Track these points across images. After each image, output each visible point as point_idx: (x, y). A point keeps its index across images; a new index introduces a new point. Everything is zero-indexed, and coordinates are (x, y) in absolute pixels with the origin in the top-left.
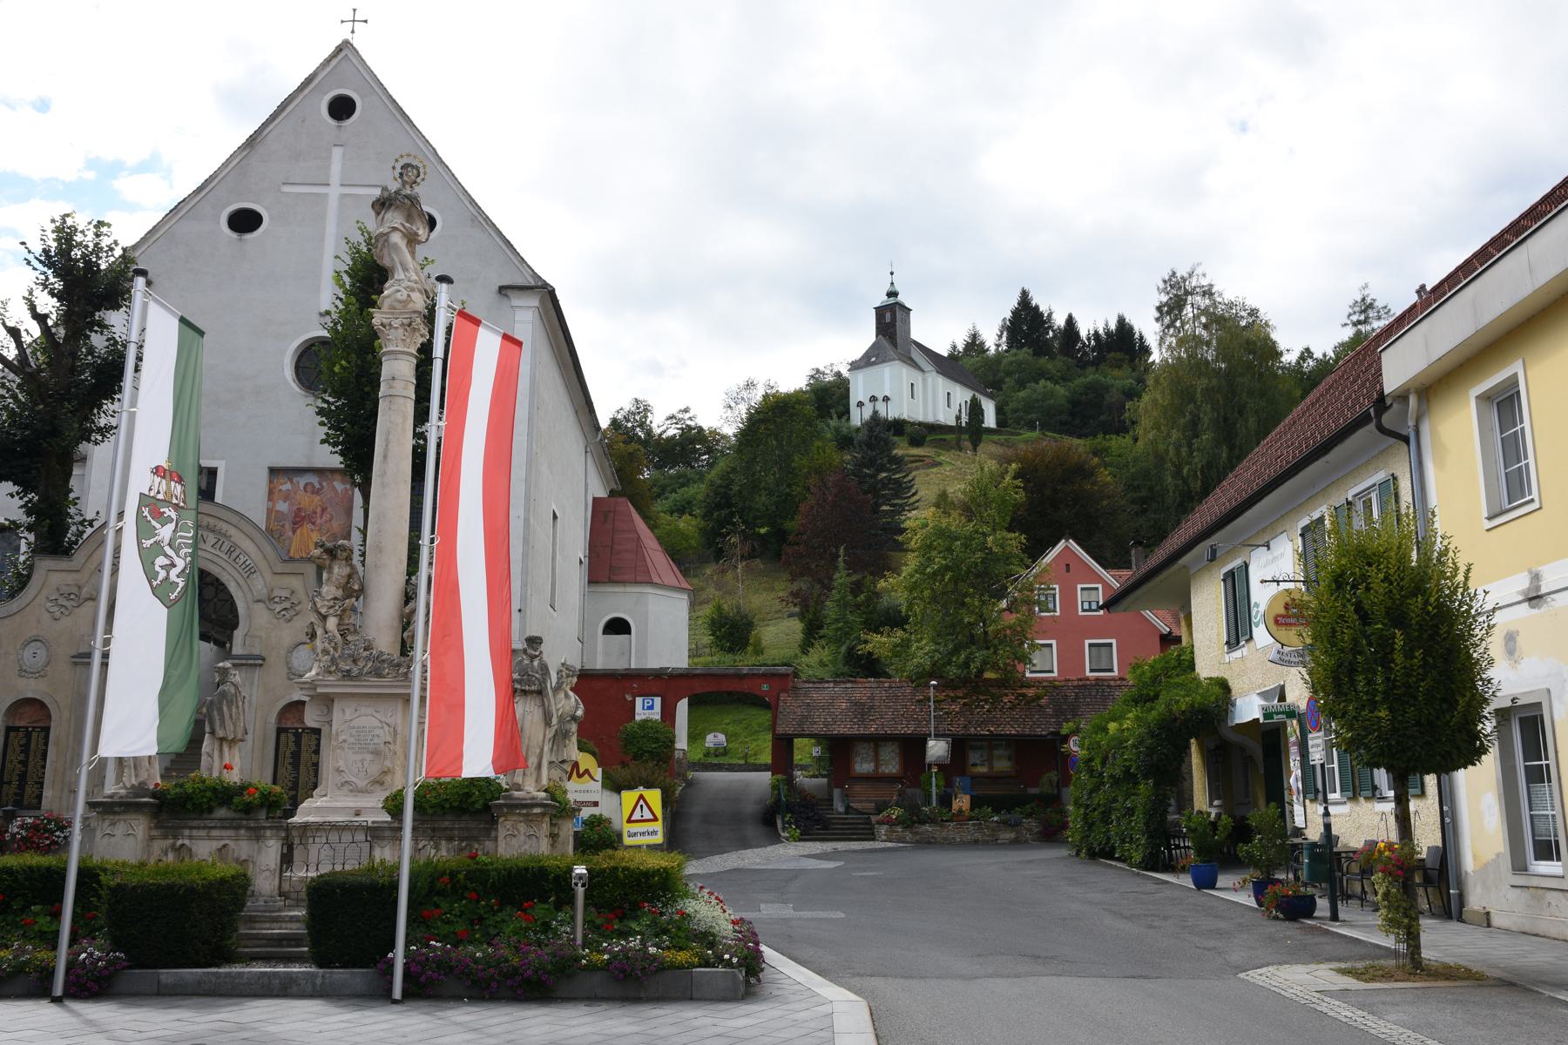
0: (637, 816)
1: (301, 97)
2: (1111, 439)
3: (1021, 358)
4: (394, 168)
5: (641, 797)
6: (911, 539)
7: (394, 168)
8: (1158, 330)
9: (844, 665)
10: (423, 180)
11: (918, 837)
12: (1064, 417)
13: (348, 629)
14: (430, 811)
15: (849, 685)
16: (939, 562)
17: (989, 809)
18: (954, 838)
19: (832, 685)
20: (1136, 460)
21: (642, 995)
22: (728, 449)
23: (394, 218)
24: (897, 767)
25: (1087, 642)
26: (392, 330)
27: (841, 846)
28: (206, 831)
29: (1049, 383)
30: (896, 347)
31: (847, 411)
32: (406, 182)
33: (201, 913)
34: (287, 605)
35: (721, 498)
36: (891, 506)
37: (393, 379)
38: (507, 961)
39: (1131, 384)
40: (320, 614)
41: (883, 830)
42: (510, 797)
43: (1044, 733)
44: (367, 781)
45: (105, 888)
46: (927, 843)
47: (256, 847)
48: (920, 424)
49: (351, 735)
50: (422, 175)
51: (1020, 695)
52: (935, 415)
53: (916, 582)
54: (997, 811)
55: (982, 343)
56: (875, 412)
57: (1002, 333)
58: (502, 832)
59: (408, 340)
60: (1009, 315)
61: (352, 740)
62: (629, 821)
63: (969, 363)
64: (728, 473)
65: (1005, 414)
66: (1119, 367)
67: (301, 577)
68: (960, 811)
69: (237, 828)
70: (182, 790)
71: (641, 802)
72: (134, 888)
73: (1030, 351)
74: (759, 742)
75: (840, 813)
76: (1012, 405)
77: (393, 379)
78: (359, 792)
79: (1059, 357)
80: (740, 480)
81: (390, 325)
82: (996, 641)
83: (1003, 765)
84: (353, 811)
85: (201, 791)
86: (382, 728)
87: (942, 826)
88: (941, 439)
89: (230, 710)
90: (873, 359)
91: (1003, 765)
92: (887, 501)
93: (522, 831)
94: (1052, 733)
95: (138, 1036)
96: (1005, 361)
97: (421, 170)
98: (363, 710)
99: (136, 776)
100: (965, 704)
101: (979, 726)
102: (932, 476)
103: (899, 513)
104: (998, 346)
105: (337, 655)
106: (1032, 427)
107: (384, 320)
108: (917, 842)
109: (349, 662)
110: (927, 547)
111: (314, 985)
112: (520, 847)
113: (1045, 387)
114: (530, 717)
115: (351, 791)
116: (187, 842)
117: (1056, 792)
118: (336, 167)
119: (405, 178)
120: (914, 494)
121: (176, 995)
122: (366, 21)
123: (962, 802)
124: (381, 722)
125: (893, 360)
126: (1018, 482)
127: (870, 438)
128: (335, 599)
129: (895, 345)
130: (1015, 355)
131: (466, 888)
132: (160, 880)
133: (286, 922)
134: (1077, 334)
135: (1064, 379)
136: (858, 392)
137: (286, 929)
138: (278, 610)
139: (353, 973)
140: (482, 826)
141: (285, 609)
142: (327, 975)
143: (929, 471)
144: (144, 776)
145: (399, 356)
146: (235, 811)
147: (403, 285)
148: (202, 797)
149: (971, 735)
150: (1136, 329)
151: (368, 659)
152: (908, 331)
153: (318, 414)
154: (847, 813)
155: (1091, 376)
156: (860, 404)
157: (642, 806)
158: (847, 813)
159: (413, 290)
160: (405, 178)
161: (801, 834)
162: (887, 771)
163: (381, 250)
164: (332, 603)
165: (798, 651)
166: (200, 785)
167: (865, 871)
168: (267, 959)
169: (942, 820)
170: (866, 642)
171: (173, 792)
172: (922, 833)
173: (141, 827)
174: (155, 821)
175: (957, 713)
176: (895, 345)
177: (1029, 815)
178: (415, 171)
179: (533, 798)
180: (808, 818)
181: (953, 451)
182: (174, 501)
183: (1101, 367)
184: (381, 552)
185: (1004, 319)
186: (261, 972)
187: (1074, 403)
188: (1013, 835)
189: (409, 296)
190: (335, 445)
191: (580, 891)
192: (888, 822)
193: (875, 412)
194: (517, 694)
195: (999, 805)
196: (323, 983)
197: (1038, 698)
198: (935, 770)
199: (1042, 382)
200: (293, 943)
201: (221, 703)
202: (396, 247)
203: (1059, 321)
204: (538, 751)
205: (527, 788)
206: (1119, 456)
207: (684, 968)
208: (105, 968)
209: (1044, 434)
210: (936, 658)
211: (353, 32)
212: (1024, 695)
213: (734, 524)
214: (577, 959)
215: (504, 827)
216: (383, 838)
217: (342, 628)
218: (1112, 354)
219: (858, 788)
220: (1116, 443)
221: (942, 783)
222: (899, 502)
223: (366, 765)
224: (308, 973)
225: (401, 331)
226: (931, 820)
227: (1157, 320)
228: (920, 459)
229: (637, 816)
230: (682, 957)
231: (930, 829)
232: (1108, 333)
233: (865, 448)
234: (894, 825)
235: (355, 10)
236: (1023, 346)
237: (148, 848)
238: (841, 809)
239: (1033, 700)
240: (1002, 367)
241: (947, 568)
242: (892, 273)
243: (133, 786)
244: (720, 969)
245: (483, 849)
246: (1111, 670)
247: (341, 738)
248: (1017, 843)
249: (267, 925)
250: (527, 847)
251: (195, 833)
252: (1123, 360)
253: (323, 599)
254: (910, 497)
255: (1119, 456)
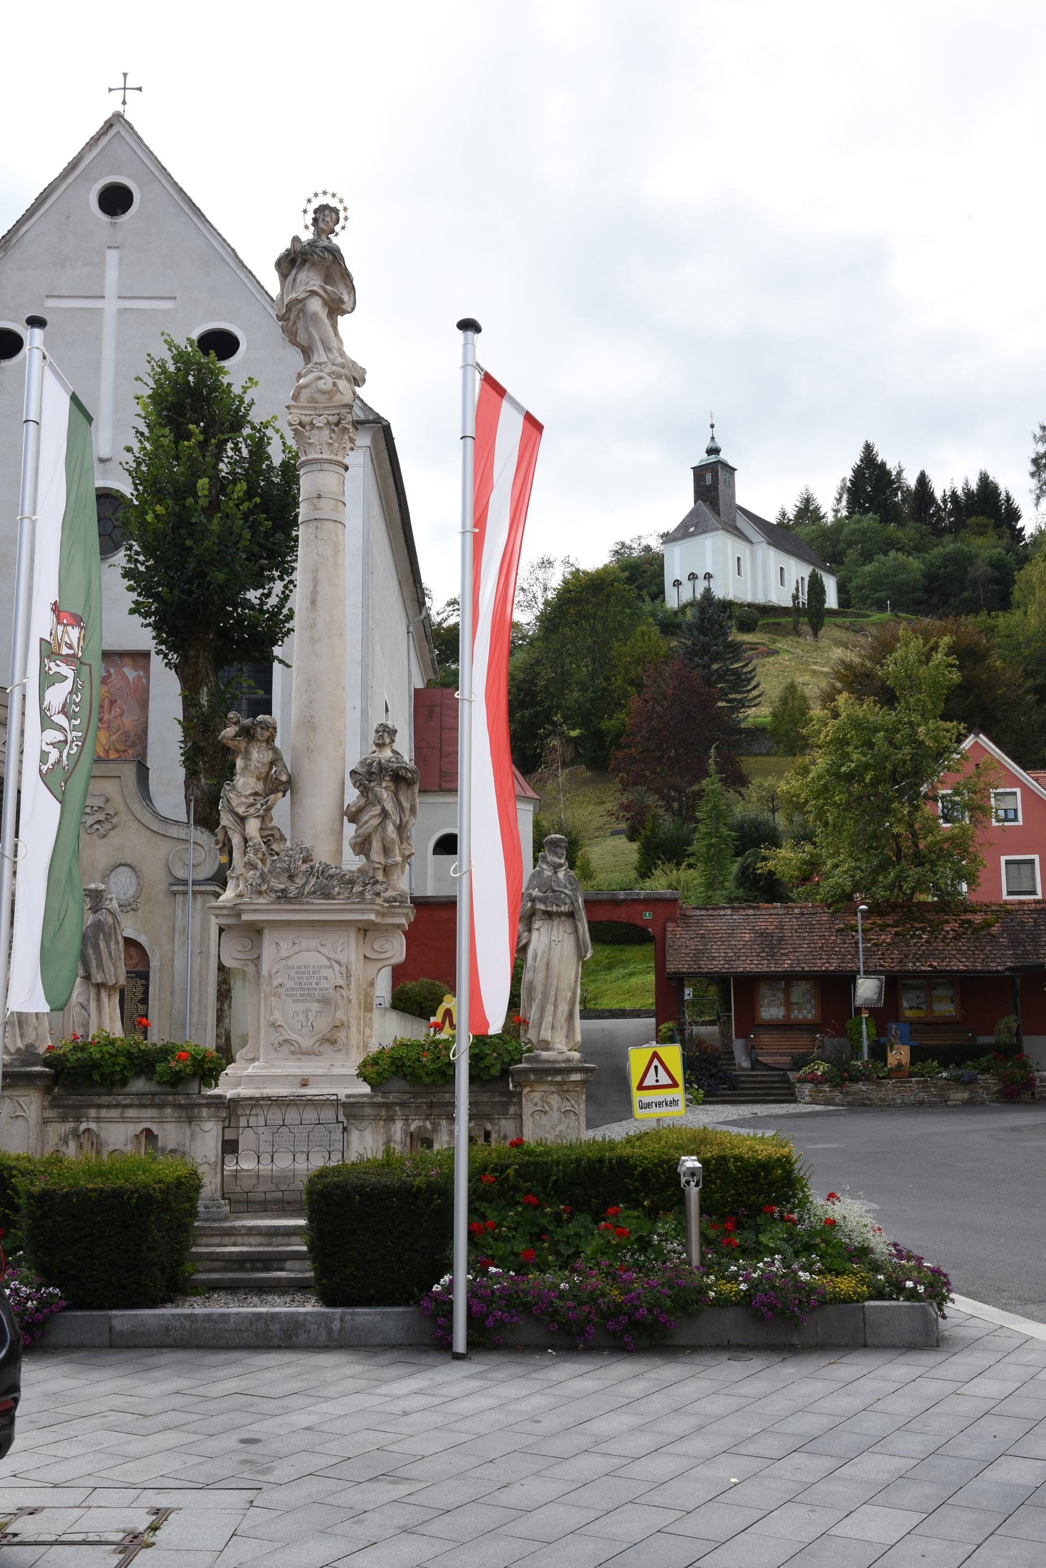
0: (650, 1081)
1: (63, 186)
2: (998, 617)
3: (866, 525)
4: (305, 211)
5: (655, 1055)
6: (820, 732)
7: (305, 211)
8: (1033, 488)
9: (737, 888)
10: (343, 228)
11: (850, 1098)
12: (919, 595)
13: (272, 835)
14: (427, 1080)
15: (750, 912)
16: (858, 759)
17: (935, 1063)
18: (894, 1099)
19: (729, 912)
20: (1029, 641)
21: (795, 1341)
22: (520, 639)
23: (309, 279)
24: (813, 1011)
25: (1003, 859)
26: (315, 432)
27: (760, 1109)
28: (119, 1110)
29: (900, 554)
30: (719, 514)
31: (661, 592)
32: (323, 230)
33: (159, 1231)
34: (101, 816)
35: (526, 695)
36: (728, 701)
37: (319, 496)
38: (603, 1295)
39: (1000, 554)
40: (237, 814)
41: (807, 1089)
42: (536, 1059)
43: (1000, 968)
44: (314, 1039)
45: (22, 1194)
46: (861, 1105)
47: (188, 1132)
48: (750, 605)
49: (290, 978)
50: (342, 222)
51: (965, 922)
52: (766, 596)
53: (825, 785)
54: (944, 1065)
55: (817, 509)
56: (708, 590)
57: (841, 497)
58: (527, 1109)
59: (336, 445)
60: (849, 474)
61: (290, 984)
62: (640, 1087)
63: (806, 530)
64: (532, 665)
65: (847, 593)
66: (982, 534)
67: (117, 780)
68: (900, 1065)
69: (161, 1106)
70: (85, 1055)
71: (656, 1062)
72: (66, 1196)
73: (877, 517)
74: (598, 984)
75: (744, 1069)
76: (856, 582)
77: (319, 496)
78: (303, 1054)
79: (911, 523)
80: (546, 674)
81: (311, 423)
82: (933, 857)
83: (945, 1008)
84: (298, 1080)
85: (111, 1055)
86: (331, 967)
87: (878, 1084)
88: (775, 624)
89: (108, 946)
90: (692, 529)
91: (945, 1008)
92: (723, 695)
93: (555, 1107)
94: (1010, 968)
95: (105, 1414)
96: (846, 531)
97: (342, 215)
98: (304, 943)
99: (22, 1036)
100: (897, 934)
101: (918, 960)
102: (769, 666)
103: (737, 709)
104: (836, 511)
105: (266, 870)
106: (881, 607)
107: (304, 418)
108: (849, 1104)
109: (284, 878)
110: (840, 743)
111: (330, 1331)
112: (553, 1128)
113: (895, 559)
114: (558, 948)
115: (292, 1053)
116: (93, 1126)
117: (1015, 1041)
118: (112, 276)
119: (322, 225)
120: (754, 688)
121: (136, 1347)
122: (140, 89)
123: (899, 1055)
124: (329, 959)
125: (716, 529)
126: (951, 659)
127: (703, 621)
128: (256, 794)
129: (717, 512)
130: (859, 521)
131: (516, 1189)
132: (98, 1183)
133: (243, 1235)
134: (931, 496)
135: (918, 549)
136: (675, 569)
137: (243, 1245)
138: (89, 823)
139: (383, 1314)
140: (497, 1099)
141: (99, 822)
142: (348, 1317)
143: (765, 660)
144: (31, 1037)
145: (325, 466)
146: (158, 1082)
147: (327, 370)
148: (114, 1064)
149: (909, 971)
150: (1002, 488)
151: (311, 871)
152: (732, 496)
153: (124, 576)
154: (753, 1069)
155: (949, 546)
156: (677, 583)
157: (656, 1068)
158: (753, 1069)
159: (339, 376)
160: (322, 225)
161: (705, 1096)
162: (801, 1017)
163: (295, 323)
164: (251, 800)
165: (633, 875)
166: (109, 1048)
167: (816, 1143)
168: (232, 1288)
169: (878, 1077)
170: (765, 859)
171: (72, 1058)
172: (855, 1093)
173: (33, 1107)
174: (50, 1098)
175: (889, 944)
176: (717, 512)
177: (985, 1070)
178: (334, 215)
179: (568, 1061)
180: (711, 1076)
181: (790, 637)
182: (65, 651)
183: (962, 534)
184: (314, 729)
185: (844, 480)
186: (254, 1314)
187: (931, 578)
188: (966, 1095)
189: (335, 384)
190: (146, 616)
191: (694, 1192)
192: (812, 1079)
193: (708, 590)
194: (537, 917)
195: (947, 1057)
196: (342, 1329)
197: (988, 925)
198: (865, 1015)
199: (892, 554)
200: (259, 1265)
201: (96, 937)
202: (315, 318)
203: (911, 481)
204: (569, 995)
205: (558, 1046)
206: (1009, 637)
207: (851, 1301)
208: (37, 1309)
209: (897, 616)
210: (857, 878)
211: (124, 103)
212: (969, 922)
213: (554, 724)
214: (702, 1290)
215: (532, 1099)
216: (362, 1118)
217: (265, 833)
218: (974, 518)
219: (766, 1038)
220: (1002, 620)
221: (874, 1031)
222: (739, 696)
223: (311, 1018)
224: (322, 1314)
225: (326, 432)
226: (866, 1078)
227: (1033, 475)
228: (753, 647)
229: (650, 1081)
230: (845, 1284)
231: (864, 1088)
232: (968, 493)
233: (696, 632)
234: (821, 1083)
235: (125, 75)
236: (866, 511)
237: (42, 1140)
238: (746, 1064)
239: (982, 928)
240: (842, 537)
241: (867, 766)
242: (712, 426)
243: (18, 1050)
244: (902, 1303)
245: (499, 1132)
246: (1034, 893)
247: (276, 982)
248: (972, 1105)
249: (216, 1240)
250: (562, 1127)
251: (104, 1113)
252: (986, 526)
253: (239, 795)
254: (750, 691)
255: (1009, 637)
